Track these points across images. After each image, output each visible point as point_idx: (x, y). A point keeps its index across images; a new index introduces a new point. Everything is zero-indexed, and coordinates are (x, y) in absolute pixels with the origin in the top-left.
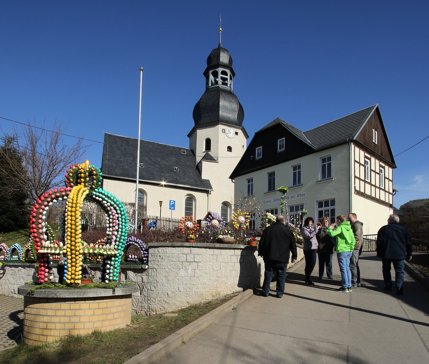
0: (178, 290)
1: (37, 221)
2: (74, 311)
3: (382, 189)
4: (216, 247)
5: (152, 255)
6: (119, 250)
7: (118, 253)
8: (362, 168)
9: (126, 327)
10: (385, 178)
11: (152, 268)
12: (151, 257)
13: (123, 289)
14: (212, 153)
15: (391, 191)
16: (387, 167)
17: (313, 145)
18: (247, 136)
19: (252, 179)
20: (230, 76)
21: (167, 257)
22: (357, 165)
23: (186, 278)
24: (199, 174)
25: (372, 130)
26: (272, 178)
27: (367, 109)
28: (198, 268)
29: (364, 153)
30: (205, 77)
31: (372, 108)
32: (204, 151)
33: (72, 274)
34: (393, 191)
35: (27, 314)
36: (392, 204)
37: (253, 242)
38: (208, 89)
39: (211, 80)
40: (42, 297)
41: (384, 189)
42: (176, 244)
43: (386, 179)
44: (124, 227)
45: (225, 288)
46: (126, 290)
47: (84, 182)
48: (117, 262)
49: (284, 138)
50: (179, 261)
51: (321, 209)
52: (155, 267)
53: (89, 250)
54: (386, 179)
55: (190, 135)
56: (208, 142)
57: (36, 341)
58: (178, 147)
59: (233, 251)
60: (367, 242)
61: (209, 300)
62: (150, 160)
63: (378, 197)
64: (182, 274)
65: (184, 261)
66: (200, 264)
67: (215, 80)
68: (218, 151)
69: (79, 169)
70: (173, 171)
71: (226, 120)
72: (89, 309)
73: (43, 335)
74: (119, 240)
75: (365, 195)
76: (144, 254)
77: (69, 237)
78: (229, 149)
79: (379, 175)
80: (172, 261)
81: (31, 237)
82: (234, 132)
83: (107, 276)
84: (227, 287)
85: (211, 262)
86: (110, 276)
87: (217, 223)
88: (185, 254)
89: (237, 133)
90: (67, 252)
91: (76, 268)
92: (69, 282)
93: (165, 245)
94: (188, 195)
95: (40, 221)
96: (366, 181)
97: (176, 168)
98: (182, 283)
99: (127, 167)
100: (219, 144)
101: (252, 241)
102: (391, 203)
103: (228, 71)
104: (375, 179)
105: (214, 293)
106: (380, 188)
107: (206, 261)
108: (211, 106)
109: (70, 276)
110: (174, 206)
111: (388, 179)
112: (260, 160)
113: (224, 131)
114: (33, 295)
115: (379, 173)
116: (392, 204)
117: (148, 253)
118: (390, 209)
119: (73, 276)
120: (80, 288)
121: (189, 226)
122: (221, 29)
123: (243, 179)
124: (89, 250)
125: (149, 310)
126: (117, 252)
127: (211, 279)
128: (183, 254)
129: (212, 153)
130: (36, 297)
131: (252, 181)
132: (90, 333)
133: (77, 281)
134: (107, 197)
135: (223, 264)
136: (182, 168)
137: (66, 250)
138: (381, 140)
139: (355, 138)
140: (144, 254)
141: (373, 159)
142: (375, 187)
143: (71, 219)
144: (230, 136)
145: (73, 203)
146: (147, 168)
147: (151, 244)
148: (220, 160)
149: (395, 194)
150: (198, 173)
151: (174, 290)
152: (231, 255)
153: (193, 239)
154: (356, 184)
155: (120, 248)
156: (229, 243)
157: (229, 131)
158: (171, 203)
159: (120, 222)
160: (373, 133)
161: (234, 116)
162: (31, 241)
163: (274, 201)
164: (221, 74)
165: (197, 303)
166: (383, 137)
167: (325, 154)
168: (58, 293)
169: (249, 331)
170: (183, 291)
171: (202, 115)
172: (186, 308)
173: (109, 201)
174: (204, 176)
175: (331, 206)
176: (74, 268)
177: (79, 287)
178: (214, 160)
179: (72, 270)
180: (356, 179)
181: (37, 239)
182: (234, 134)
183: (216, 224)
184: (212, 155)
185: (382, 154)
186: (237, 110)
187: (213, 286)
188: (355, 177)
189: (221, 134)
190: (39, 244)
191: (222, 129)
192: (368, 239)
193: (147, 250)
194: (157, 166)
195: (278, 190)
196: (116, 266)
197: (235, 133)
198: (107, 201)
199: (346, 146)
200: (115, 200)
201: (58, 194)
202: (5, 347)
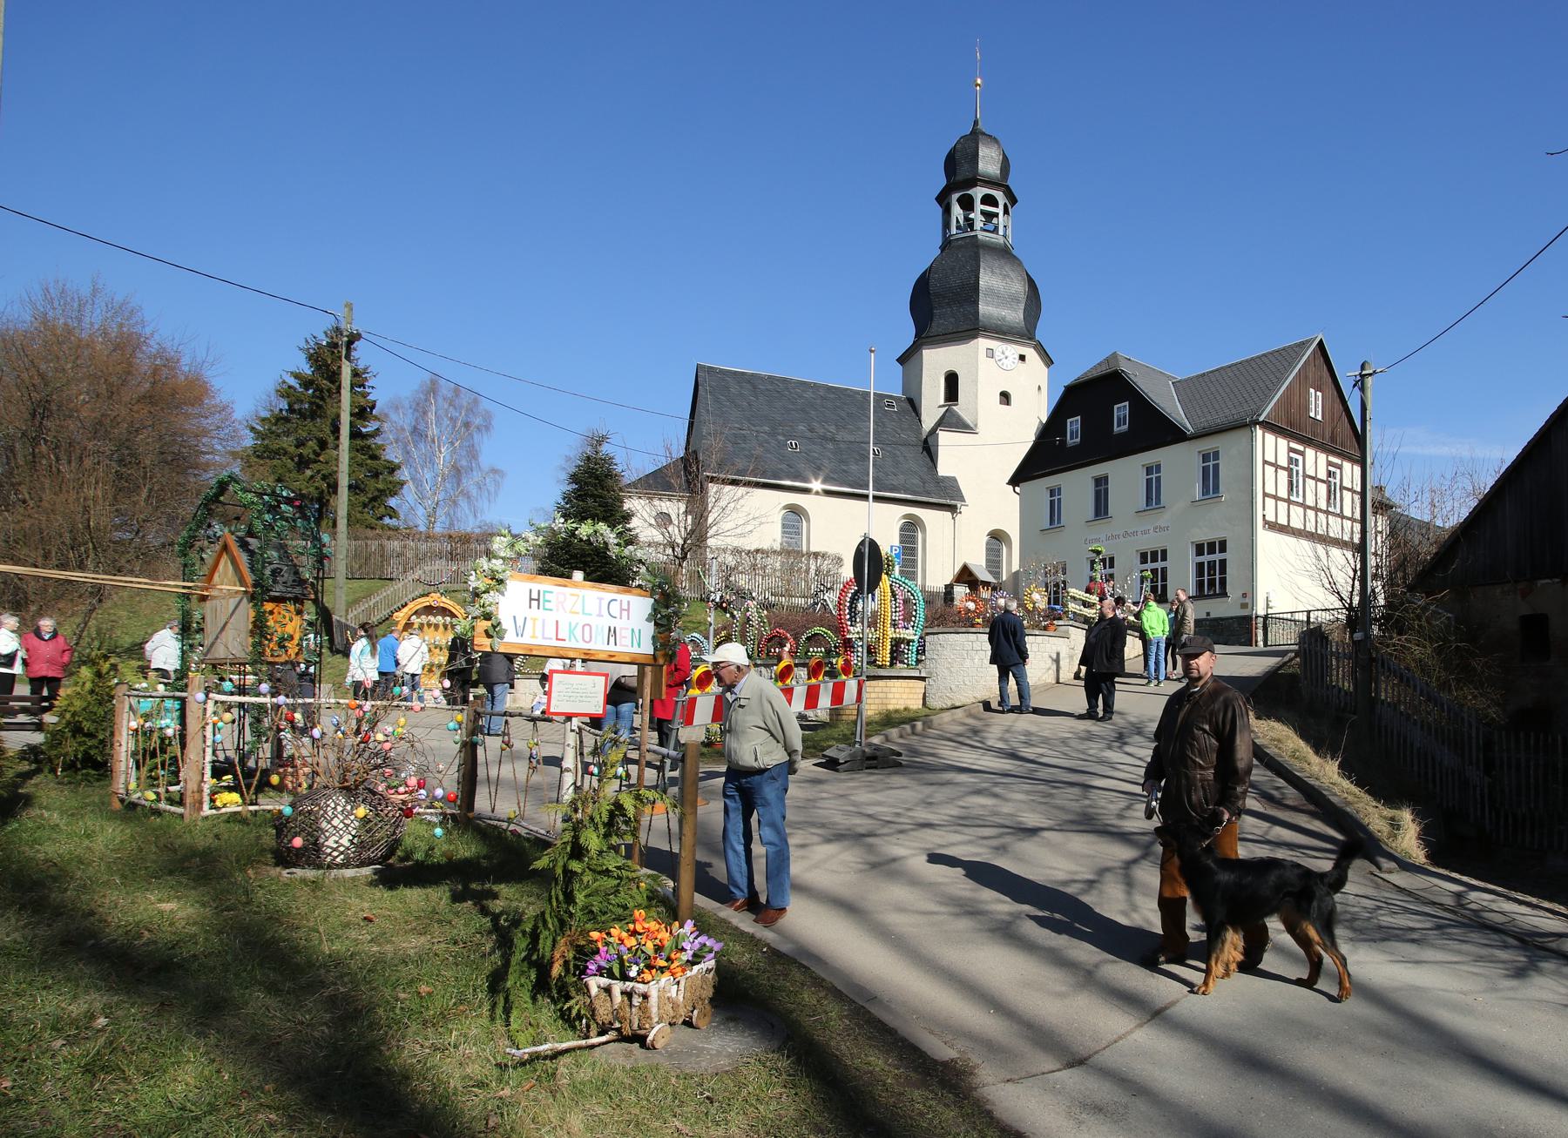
3: (1334, 514)
14: (961, 409)
19: (1059, 489)
20: (1005, 205)
24: (931, 464)
25: (1308, 393)
26: (1102, 488)
31: (1310, 342)
32: (942, 402)
38: (947, 244)
51: (1200, 559)
55: (903, 360)
56: (952, 380)
60: (1293, 627)
62: (812, 430)
67: (967, 219)
68: (976, 404)
71: (997, 325)
94: (906, 516)
99: (759, 451)
103: (999, 195)
112: (1075, 447)
113: (990, 353)
123: (1040, 486)
138: (1333, 407)
141: (1310, 453)
142: (1317, 510)
150: (928, 459)
154: (1267, 510)
157: (1003, 353)
161: (1014, 315)
164: (982, 203)
167: (1207, 445)
174: (943, 470)
186: (1023, 298)
188: (1265, 495)
192: (1295, 621)
197: (1017, 357)
199: (1246, 432)
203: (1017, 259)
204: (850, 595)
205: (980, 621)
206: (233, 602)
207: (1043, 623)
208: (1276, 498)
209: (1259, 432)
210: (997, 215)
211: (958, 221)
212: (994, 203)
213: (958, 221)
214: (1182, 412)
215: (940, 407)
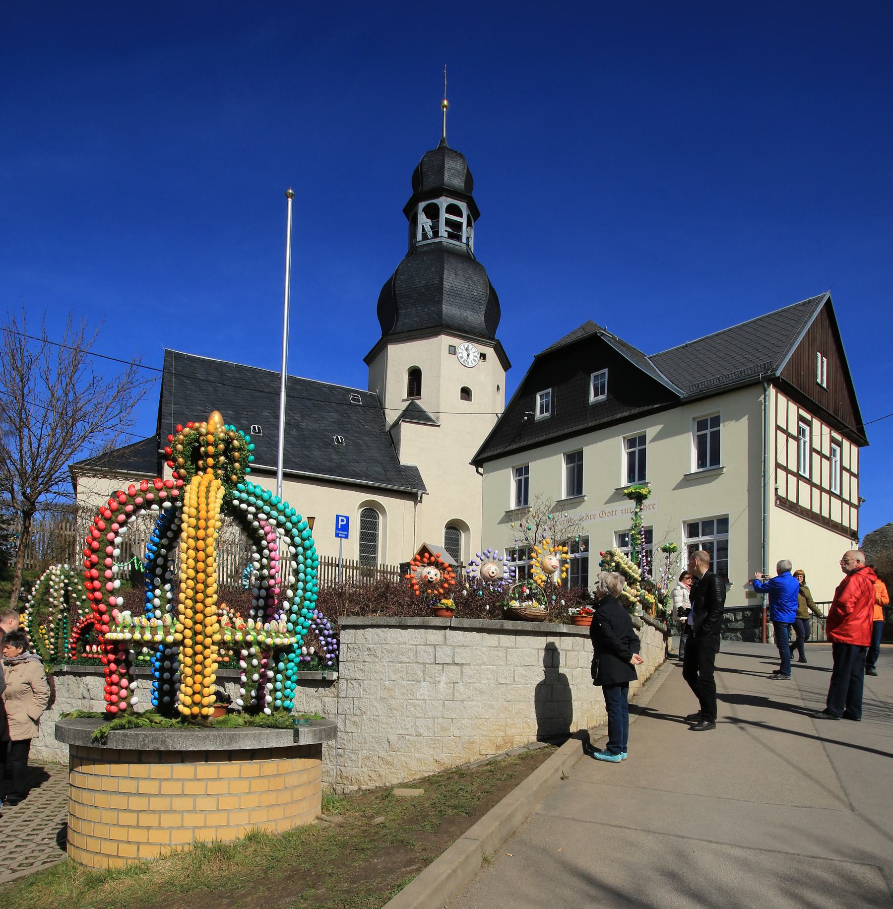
0: (413, 733)
1: (101, 561)
2: (203, 783)
4: (506, 628)
5: (348, 647)
6: (297, 633)
7: (296, 643)
9: (316, 821)
10: (843, 468)
11: (348, 677)
12: (345, 651)
13: (315, 730)
15: (855, 501)
18: (506, 365)
21: (388, 652)
22: (782, 437)
23: (434, 702)
25: (817, 354)
28: (462, 679)
30: (408, 219)
32: (405, 397)
33: (194, 693)
34: (859, 499)
35: (75, 787)
36: (856, 530)
37: (586, 617)
38: (413, 250)
39: (423, 226)
40: (128, 748)
41: (839, 494)
42: (410, 621)
43: (843, 471)
44: (309, 577)
45: (523, 728)
46: (320, 731)
47: (214, 467)
48: (292, 664)
49: (606, 370)
50: (416, 663)
52: (357, 676)
53: (233, 634)
54: (843, 471)
56: (415, 375)
57: (108, 856)
59: (512, 637)
61: (489, 757)
63: (825, 514)
64: (424, 694)
65: (428, 661)
66: (466, 669)
69: (201, 435)
70: (330, 445)
72: (240, 778)
73: (129, 842)
74: (299, 609)
75: (799, 508)
76: (327, 644)
77: (189, 603)
79: (828, 462)
80: (401, 662)
81: (28, 601)
82: (476, 354)
83: (269, 698)
84: (529, 725)
85: (493, 665)
86: (276, 699)
87: (496, 570)
88: (431, 645)
89: (483, 356)
90: (184, 638)
91: (205, 677)
92: (186, 711)
93: (382, 623)
95: (108, 561)
96: (801, 475)
97: (337, 437)
98: (423, 715)
101: (584, 615)
102: (854, 527)
104: (821, 471)
105: (499, 739)
106: (830, 493)
107: (480, 662)
108: (423, 291)
109: (190, 696)
111: (848, 471)
113: (453, 350)
114: (105, 743)
115: (828, 456)
116: (856, 530)
117: (338, 643)
118: (852, 543)
119: (197, 698)
120: (211, 727)
121: (431, 578)
122: (445, 103)
124: (233, 634)
125: (340, 780)
126: (293, 640)
127: (491, 707)
128: (426, 645)
129: (423, 403)
130: (114, 748)
131: (527, 472)
132: (242, 837)
133: (207, 708)
134: (267, 502)
135: (520, 670)
136: (353, 438)
137: (182, 632)
139: (778, 374)
140: (327, 644)
141: (816, 423)
142: (822, 489)
143: (196, 557)
144: (468, 364)
145: (198, 519)
146: (269, 438)
147: (343, 621)
148: (443, 420)
151: (406, 732)
152: (538, 649)
153: (452, 610)
155: (299, 628)
158: (340, 523)
159: (302, 567)
162: (30, 609)
165: (459, 762)
166: (840, 370)
167: (705, 410)
168: (169, 740)
169: (627, 831)
170: (426, 735)
171: (400, 311)
172: (434, 776)
173: (274, 513)
174: (406, 458)
175: (717, 533)
176: (198, 677)
177: (209, 725)
178: (429, 419)
179: (195, 683)
180: (778, 469)
181: (102, 607)
182: (476, 359)
183: (493, 573)
184: (425, 408)
185: (836, 411)
186: (484, 300)
187: (498, 722)
189: (447, 360)
190: (106, 617)
191: (450, 346)
193: (335, 636)
194: (292, 432)
195: (626, 494)
196: (289, 672)
197: (478, 356)
198: (268, 514)
199: (759, 389)
200: (288, 512)
201: (150, 496)
202: (14, 871)
203: (480, 265)
205: (449, 602)
207: (571, 611)
209: (772, 391)
211: (423, 229)
213: (423, 229)
215: (403, 401)
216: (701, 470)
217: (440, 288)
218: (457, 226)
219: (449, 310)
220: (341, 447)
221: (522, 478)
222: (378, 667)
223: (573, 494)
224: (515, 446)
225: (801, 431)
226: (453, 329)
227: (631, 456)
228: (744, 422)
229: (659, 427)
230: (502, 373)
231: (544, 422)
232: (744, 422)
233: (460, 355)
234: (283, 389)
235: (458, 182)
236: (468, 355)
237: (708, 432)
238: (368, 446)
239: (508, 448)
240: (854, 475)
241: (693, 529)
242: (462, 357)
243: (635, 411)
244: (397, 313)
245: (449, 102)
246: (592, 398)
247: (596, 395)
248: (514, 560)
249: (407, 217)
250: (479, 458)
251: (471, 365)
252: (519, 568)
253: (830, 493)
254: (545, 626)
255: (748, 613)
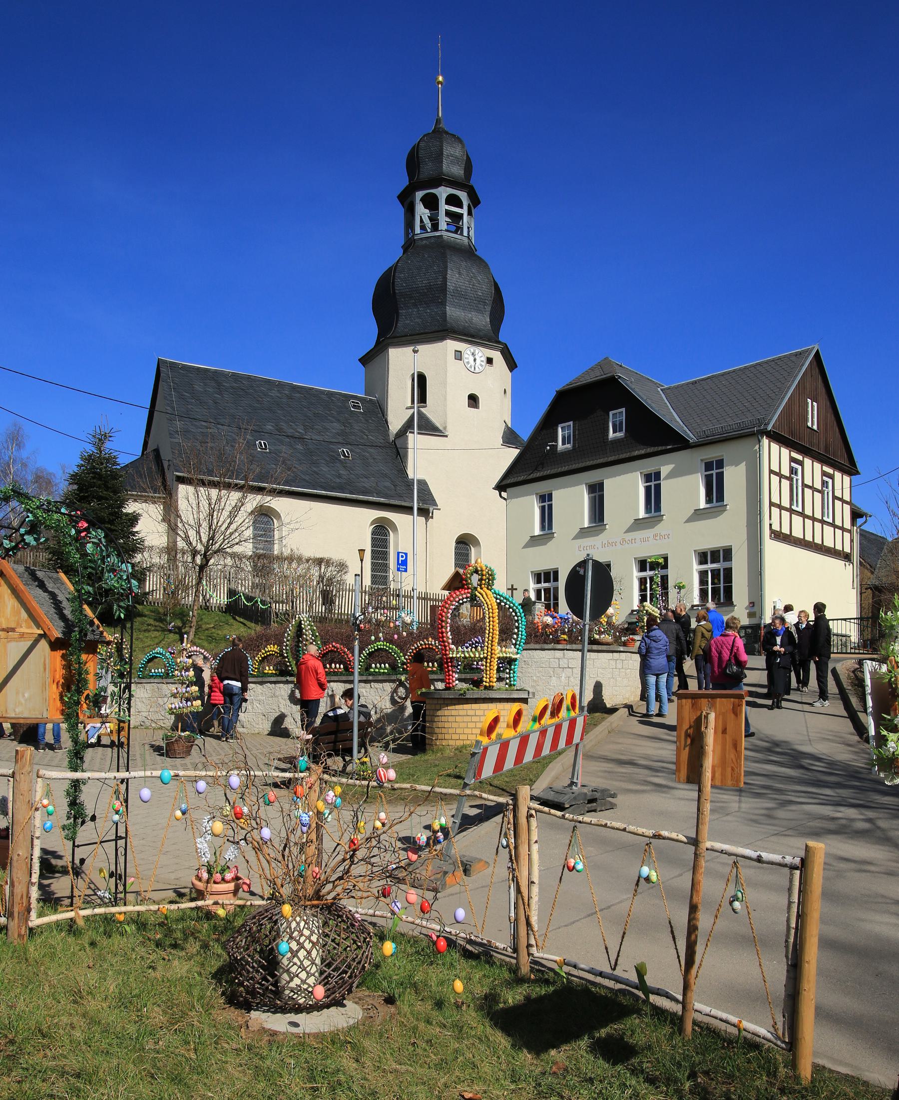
3: (828, 524)
8: (786, 484)
16: (838, 475)
17: (689, 432)
27: (796, 355)
29: (790, 451)
31: (810, 351)
38: (410, 245)
49: (623, 410)
55: (365, 360)
58: (340, 394)
59: (611, 654)
63: (818, 540)
70: (337, 459)
75: (792, 538)
78: (472, 401)
89: (490, 361)
97: (343, 451)
100: (448, 390)
102: (847, 549)
103: (463, 196)
104: (812, 503)
106: (823, 522)
108: (426, 291)
110: (405, 563)
113: (459, 355)
122: (441, 78)
139: (769, 428)
141: (808, 462)
142: (813, 519)
149: (865, 522)
156: (608, 644)
158: (400, 559)
160: (807, 407)
163: (603, 546)
164: (446, 203)
166: (830, 410)
167: (712, 453)
171: (400, 311)
173: (508, 603)
182: (483, 363)
185: (827, 449)
186: (489, 301)
188: (772, 504)
191: (456, 351)
204: (451, 611)
206: (16, 649)
207: (623, 639)
208: (780, 507)
209: (765, 441)
210: (460, 216)
211: (422, 221)
212: (459, 204)
213: (422, 221)
214: (678, 419)
216: (708, 506)
217: (443, 288)
218: (457, 217)
219: (454, 313)
220: (348, 461)
221: (546, 504)
222: (530, 670)
223: (595, 522)
224: (538, 475)
225: (793, 471)
226: (459, 334)
227: (648, 490)
228: (742, 467)
229: (671, 467)
230: (509, 374)
231: (566, 454)
232: (742, 467)
233: (466, 360)
234: (415, 487)
235: (457, 171)
236: (475, 360)
237: (714, 472)
238: (374, 459)
239: (531, 476)
240: (847, 503)
241: (703, 557)
242: (468, 363)
243: (650, 450)
244: (398, 314)
245: (444, 78)
246: (611, 435)
247: (614, 432)
248: (539, 582)
249: (402, 203)
250: (502, 484)
251: (477, 370)
252: (545, 590)
253: (823, 522)
254: (612, 648)
255: (750, 631)
